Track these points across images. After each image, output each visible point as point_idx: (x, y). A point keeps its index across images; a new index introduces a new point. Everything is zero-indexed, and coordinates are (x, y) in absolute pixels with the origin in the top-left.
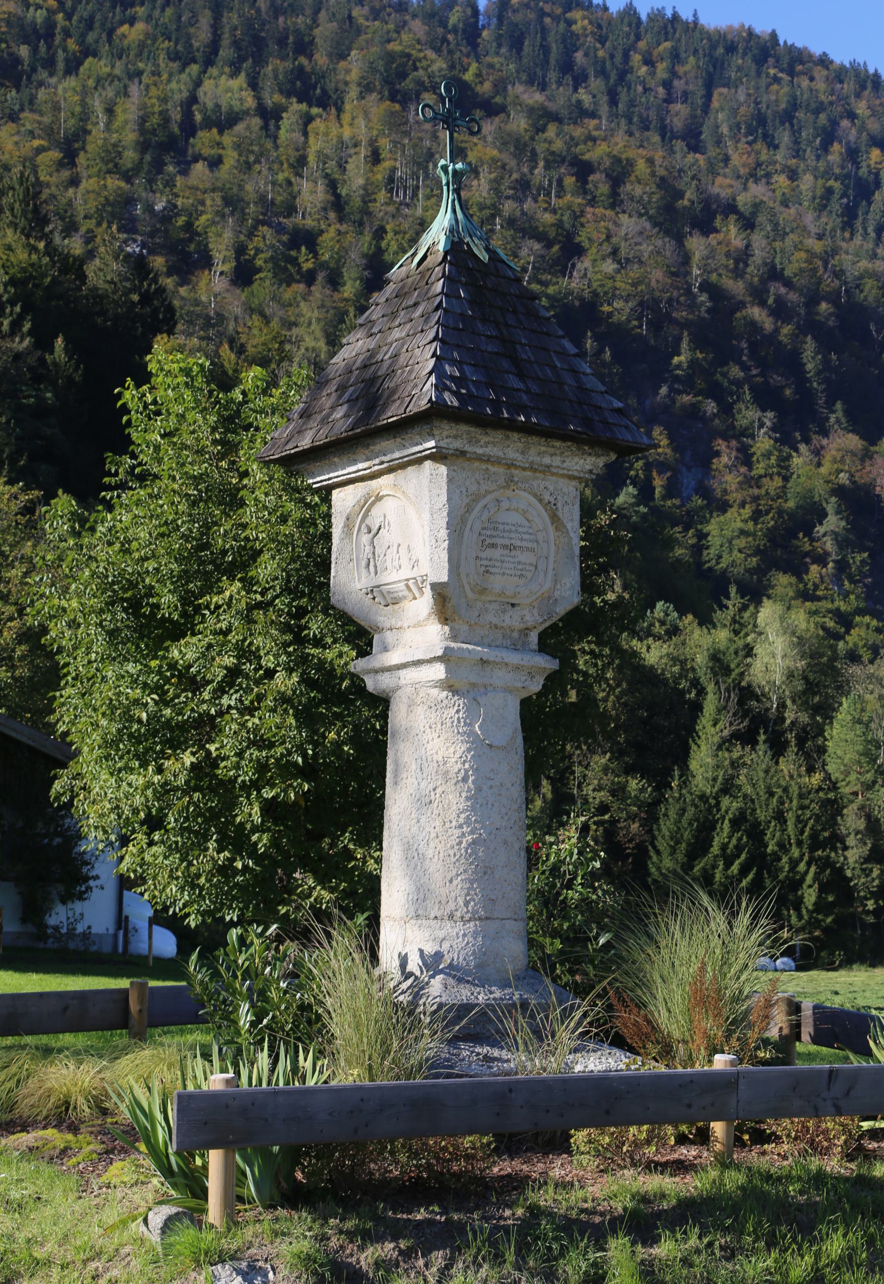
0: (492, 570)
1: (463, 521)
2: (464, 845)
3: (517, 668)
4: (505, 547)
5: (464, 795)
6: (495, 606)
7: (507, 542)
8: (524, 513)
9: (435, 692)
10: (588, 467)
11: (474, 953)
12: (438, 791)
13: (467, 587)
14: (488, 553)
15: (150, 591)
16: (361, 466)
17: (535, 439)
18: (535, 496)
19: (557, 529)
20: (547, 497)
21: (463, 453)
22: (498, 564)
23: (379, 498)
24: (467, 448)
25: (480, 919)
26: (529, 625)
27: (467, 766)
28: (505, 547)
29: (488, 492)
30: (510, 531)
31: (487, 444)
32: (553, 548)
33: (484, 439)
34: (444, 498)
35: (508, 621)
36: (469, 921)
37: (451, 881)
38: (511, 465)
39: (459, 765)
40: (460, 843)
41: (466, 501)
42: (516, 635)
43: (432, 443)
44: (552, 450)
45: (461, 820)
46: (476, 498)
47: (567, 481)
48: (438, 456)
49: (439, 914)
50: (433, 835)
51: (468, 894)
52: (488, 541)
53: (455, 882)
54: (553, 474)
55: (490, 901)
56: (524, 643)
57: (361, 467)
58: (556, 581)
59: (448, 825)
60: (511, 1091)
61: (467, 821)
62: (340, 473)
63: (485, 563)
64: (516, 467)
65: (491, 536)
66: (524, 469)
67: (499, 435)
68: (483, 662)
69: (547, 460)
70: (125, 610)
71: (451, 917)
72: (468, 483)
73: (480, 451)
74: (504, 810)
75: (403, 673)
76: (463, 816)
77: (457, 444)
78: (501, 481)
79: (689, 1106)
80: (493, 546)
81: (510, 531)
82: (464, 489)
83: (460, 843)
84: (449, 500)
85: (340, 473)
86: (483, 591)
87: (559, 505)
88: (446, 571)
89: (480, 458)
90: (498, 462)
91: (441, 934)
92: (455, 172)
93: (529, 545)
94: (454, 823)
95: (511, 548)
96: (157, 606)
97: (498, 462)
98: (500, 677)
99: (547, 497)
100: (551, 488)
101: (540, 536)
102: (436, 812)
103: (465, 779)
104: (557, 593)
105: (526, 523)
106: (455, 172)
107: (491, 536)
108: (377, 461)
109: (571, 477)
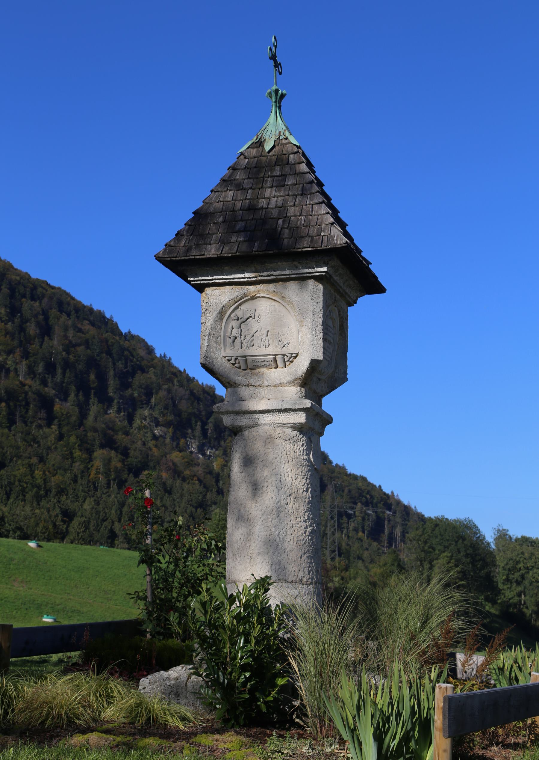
2: (307, 533)
9: (289, 431)
16: (247, 275)
19: (340, 334)
23: (253, 298)
34: (321, 305)
36: (310, 584)
37: (301, 558)
40: (305, 532)
43: (325, 269)
45: (306, 517)
48: (319, 279)
49: (294, 579)
50: (290, 526)
51: (310, 567)
57: (247, 276)
59: (299, 520)
62: (225, 277)
71: (301, 581)
75: (261, 416)
83: (305, 532)
85: (225, 277)
88: (322, 353)
94: (302, 519)
108: (266, 274)
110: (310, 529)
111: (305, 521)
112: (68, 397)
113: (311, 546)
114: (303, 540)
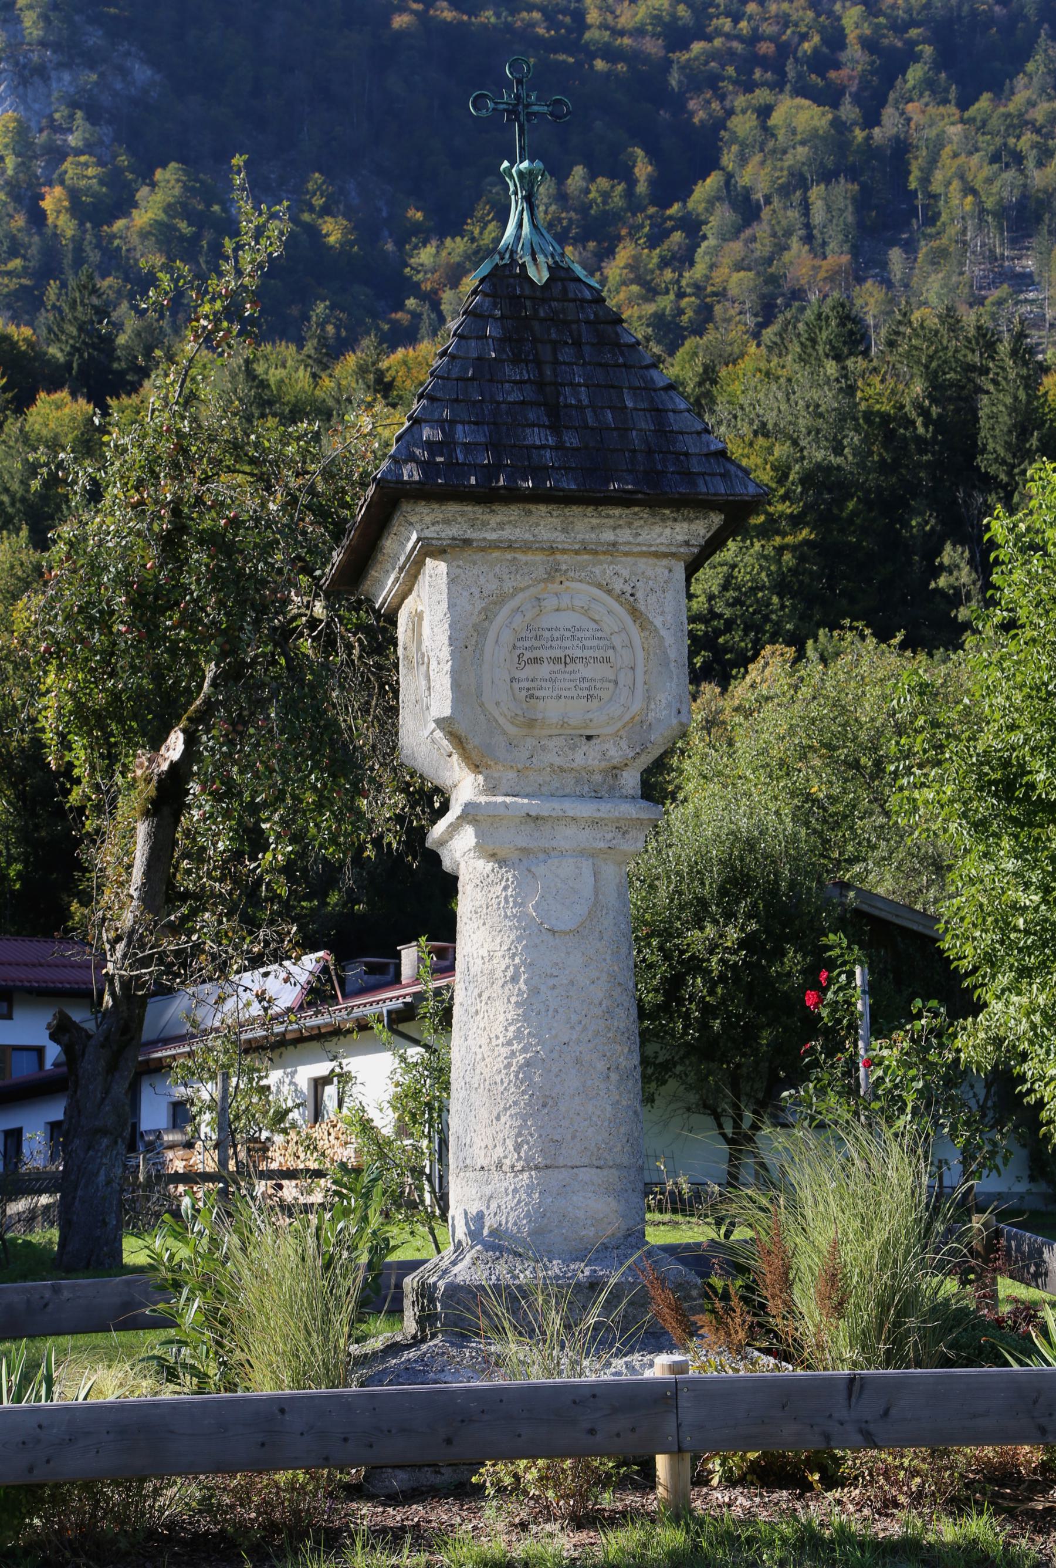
0: (538, 693)
1: (480, 630)
3: (595, 823)
4: (556, 660)
5: (513, 999)
6: (560, 742)
7: (559, 653)
8: (585, 612)
10: (680, 538)
11: (528, 1215)
12: (484, 997)
13: (501, 720)
14: (529, 671)
15: (1023, 770)
17: (576, 510)
18: (599, 586)
20: (618, 586)
21: (467, 542)
22: (549, 685)
24: (470, 534)
25: (537, 1168)
26: (615, 762)
27: (517, 960)
28: (556, 660)
29: (517, 590)
30: (562, 638)
31: (501, 526)
32: (640, 655)
33: (494, 520)
35: (579, 760)
37: (498, 1118)
38: (552, 550)
39: (507, 960)
40: (508, 1066)
41: (480, 605)
42: (598, 778)
44: (611, 522)
45: (510, 1034)
46: (500, 600)
47: (652, 561)
49: (485, 1162)
50: (479, 1056)
51: (519, 1134)
52: (528, 655)
53: (503, 1119)
54: (626, 554)
55: (551, 1144)
56: (612, 788)
58: (649, 699)
60: (282, 1411)
61: (518, 1035)
63: (526, 685)
64: (564, 551)
65: (532, 648)
66: (577, 552)
67: (514, 511)
68: (536, 819)
69: (608, 536)
70: (995, 795)
71: (499, 1166)
72: (482, 580)
73: (493, 536)
74: (574, 1018)
76: (512, 1028)
77: (453, 531)
78: (540, 572)
79: (592, 1432)
80: (536, 661)
81: (562, 638)
82: (476, 591)
84: (451, 606)
86: (531, 723)
87: (640, 595)
88: (449, 703)
89: (494, 546)
90: (527, 547)
91: (488, 1190)
92: (520, 173)
93: (598, 654)
94: (502, 1040)
95: (565, 661)
96: (1032, 786)
97: (527, 547)
98: (567, 837)
99: (618, 586)
100: (625, 573)
101: (617, 641)
102: (482, 1025)
103: (514, 979)
104: (651, 715)
105: (595, 626)
106: (520, 173)
107: (532, 648)
109: (657, 555)
110: (521, 1058)
111: (509, 1043)
112: (440, 304)
113: (524, 1093)
114: (502, 1082)
